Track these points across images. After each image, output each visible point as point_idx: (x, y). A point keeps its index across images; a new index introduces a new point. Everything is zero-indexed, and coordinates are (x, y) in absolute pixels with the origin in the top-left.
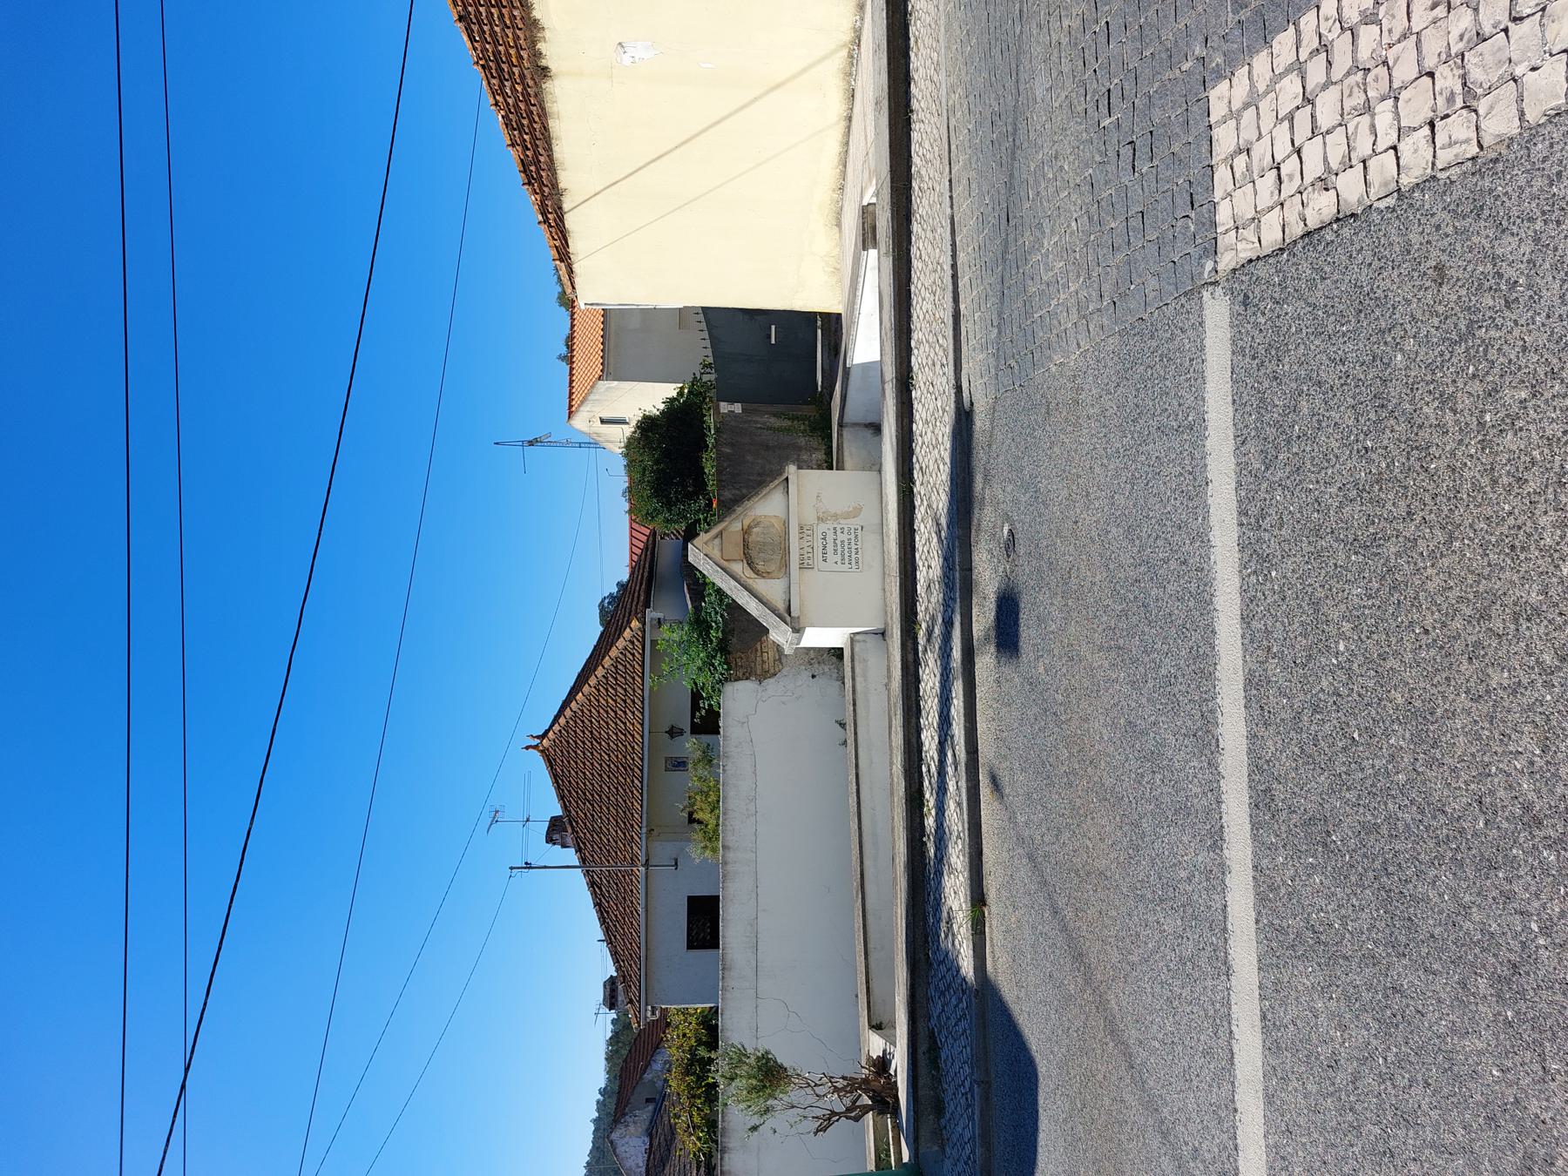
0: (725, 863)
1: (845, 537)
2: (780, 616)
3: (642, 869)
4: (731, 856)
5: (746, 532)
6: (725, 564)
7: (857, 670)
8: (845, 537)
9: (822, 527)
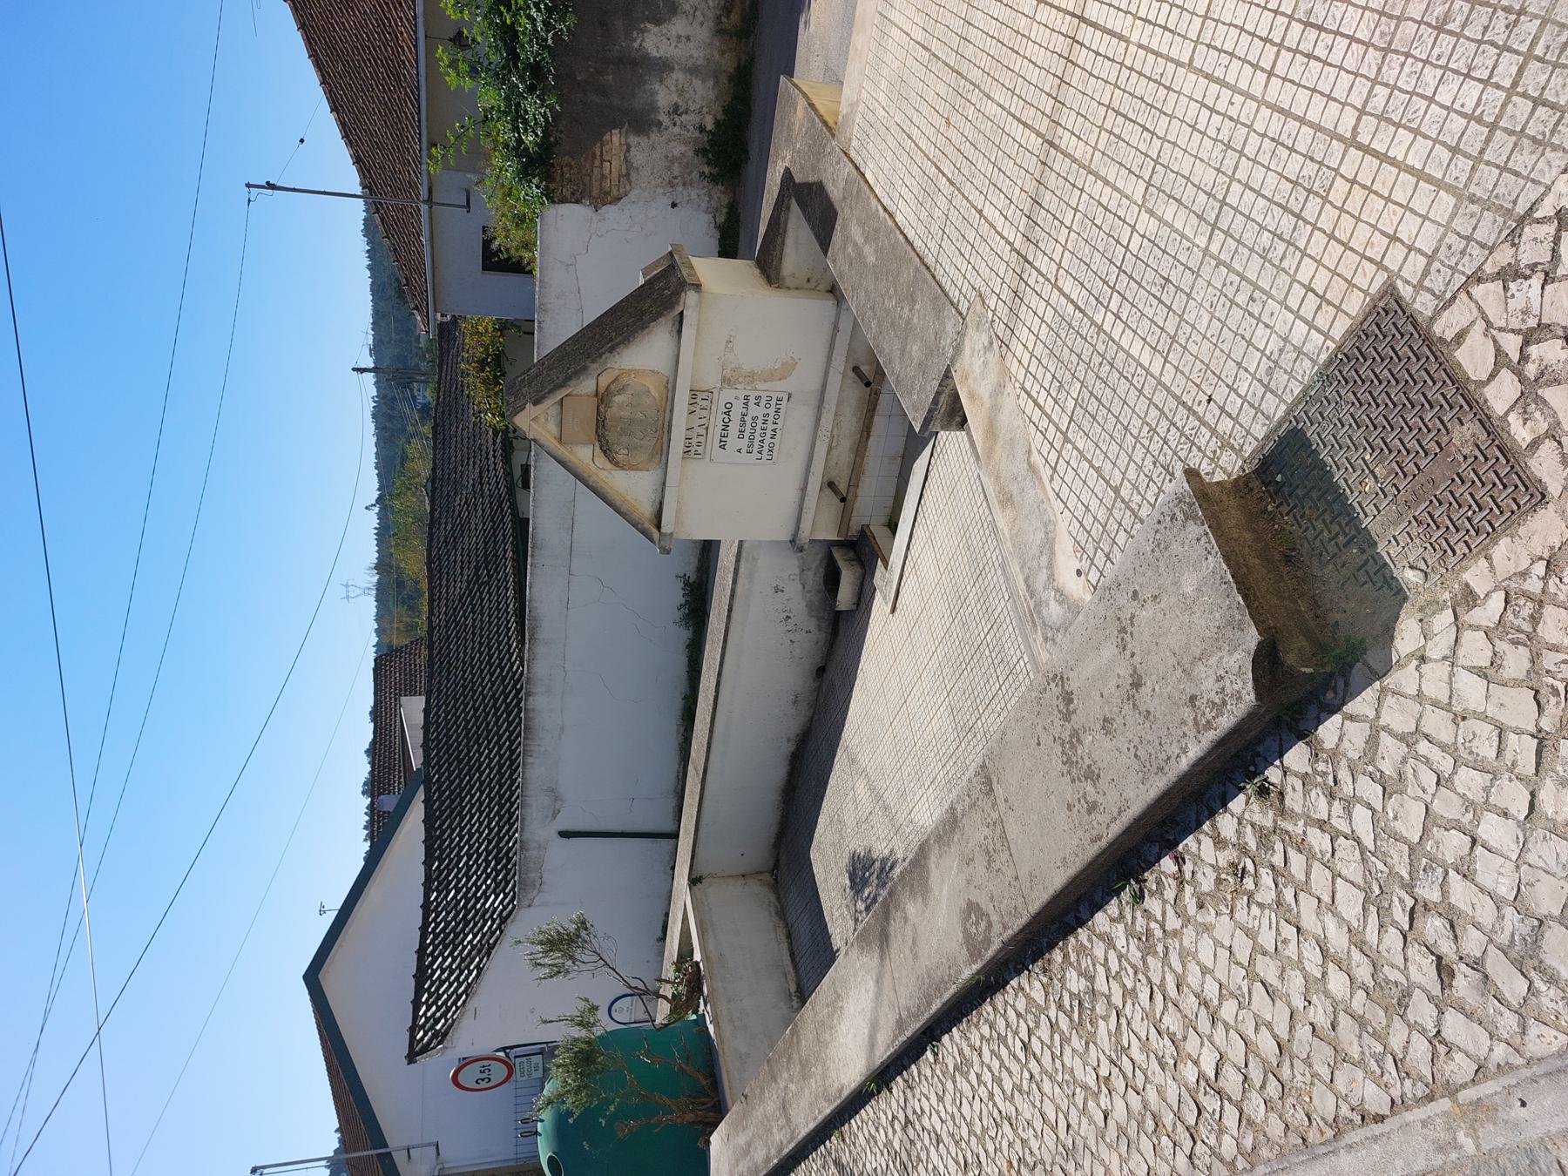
2: (645, 533)
3: (424, 208)
5: (603, 398)
6: (563, 452)
7: (742, 570)
9: (728, 395)
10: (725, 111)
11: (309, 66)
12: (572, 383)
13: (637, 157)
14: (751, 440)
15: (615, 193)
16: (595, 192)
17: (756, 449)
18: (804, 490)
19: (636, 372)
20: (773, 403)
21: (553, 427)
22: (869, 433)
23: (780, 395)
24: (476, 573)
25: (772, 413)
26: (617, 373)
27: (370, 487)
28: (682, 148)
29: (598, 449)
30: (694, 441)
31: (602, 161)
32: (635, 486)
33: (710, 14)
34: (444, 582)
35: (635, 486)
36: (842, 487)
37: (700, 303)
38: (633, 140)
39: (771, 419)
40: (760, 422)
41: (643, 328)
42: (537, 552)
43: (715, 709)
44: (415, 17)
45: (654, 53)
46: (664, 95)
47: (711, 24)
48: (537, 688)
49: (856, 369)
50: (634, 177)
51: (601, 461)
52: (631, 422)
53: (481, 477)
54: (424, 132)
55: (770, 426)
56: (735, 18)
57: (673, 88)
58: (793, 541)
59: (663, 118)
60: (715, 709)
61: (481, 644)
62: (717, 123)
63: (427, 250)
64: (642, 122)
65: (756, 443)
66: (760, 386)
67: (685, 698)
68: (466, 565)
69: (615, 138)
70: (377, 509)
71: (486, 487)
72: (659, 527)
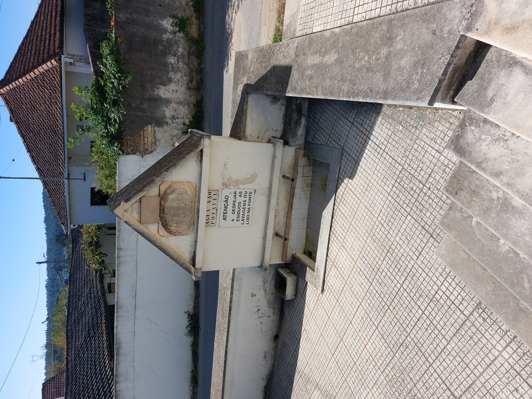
0: (119, 257)
1: (239, 199)
2: (187, 269)
3: (66, 181)
4: (122, 253)
5: (163, 197)
6: (142, 228)
7: (235, 287)
8: (239, 199)
9: (226, 192)
10: (193, 117)
11: (20, 140)
12: (146, 189)
13: (159, 135)
14: (238, 214)
15: (150, 150)
16: (141, 150)
17: (241, 219)
18: (265, 238)
19: (180, 182)
20: (248, 195)
21: (136, 215)
22: (292, 207)
23: (251, 191)
24: (88, 333)
25: (247, 200)
26: (169, 183)
27: (44, 314)
28: (177, 132)
29: (160, 226)
30: (210, 217)
31: (144, 137)
32: (180, 245)
33: (185, 82)
34: (74, 340)
35: (180, 245)
36: (282, 234)
37: (210, 145)
38: (157, 129)
39: (247, 203)
40: (242, 205)
41: (183, 158)
42: (119, 310)
43: (225, 368)
44: (62, 106)
45: (163, 96)
46: (168, 112)
47: (185, 86)
48: (121, 379)
49: (284, 177)
50: (158, 143)
51: (163, 232)
52: (178, 208)
53: (90, 291)
54: (66, 153)
55: (247, 207)
56: (194, 83)
57: (172, 109)
58: (261, 266)
59: (168, 120)
60: (225, 368)
61: (91, 365)
62: (190, 122)
63: (67, 198)
64: (160, 122)
65: (241, 216)
66: (241, 186)
67: (192, 372)
68: (84, 330)
69: (149, 128)
70: (46, 323)
71: (92, 295)
72: (194, 265)
